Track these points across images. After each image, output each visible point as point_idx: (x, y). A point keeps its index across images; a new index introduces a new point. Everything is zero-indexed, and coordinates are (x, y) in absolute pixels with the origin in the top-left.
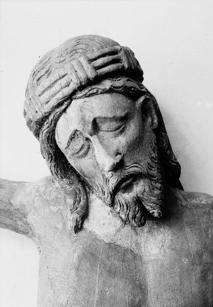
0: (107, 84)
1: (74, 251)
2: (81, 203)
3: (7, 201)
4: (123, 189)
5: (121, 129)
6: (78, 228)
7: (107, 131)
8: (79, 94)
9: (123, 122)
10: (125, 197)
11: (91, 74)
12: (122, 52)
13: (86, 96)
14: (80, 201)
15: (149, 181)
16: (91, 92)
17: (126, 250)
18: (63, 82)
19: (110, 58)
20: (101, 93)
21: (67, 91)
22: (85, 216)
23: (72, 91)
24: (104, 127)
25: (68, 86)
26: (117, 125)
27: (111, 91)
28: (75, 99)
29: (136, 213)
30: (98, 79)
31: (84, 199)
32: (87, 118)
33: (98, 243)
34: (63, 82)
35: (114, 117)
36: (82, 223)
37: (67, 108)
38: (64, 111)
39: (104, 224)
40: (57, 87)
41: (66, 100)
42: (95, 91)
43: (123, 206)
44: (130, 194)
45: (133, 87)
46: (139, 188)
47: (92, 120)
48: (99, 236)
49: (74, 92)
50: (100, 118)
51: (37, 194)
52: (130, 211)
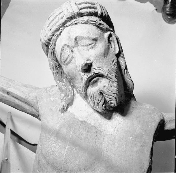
0: (86, 18)
1: (58, 123)
2: (69, 97)
3: (27, 94)
4: (92, 84)
5: (92, 45)
6: (64, 110)
7: (84, 46)
8: (69, 23)
9: (95, 42)
10: (92, 90)
11: (76, 11)
12: (98, 4)
13: (72, 25)
14: (69, 96)
15: (109, 81)
16: (75, 22)
17: (92, 126)
18: (60, 16)
19: (89, 5)
20: (82, 23)
21: (63, 21)
22: (70, 103)
23: (157, 125)
24: (81, 43)
25: (62, 18)
26: (90, 42)
27: (87, 23)
28: (67, 26)
29: (99, 101)
30: (81, 15)
31: (71, 95)
32: (72, 37)
33: (75, 119)
34: (60, 16)
35: (88, 37)
36: (67, 108)
37: (61, 32)
38: (60, 34)
39: (81, 110)
40: (57, 19)
41: (61, 27)
42: (78, 22)
43: (91, 96)
44: (96, 88)
45: (102, 24)
46: (102, 83)
47: (74, 37)
48: (76, 117)
49: (65, 23)
50: (79, 37)
51: (45, 91)
52: (95, 100)
